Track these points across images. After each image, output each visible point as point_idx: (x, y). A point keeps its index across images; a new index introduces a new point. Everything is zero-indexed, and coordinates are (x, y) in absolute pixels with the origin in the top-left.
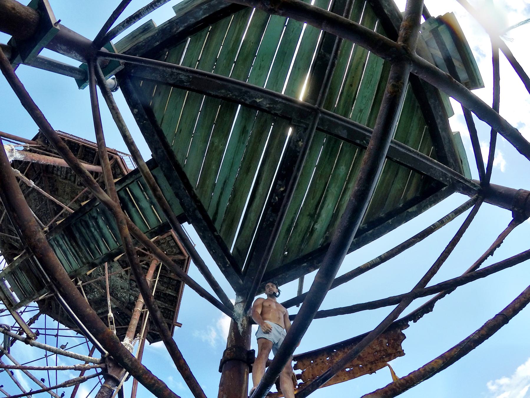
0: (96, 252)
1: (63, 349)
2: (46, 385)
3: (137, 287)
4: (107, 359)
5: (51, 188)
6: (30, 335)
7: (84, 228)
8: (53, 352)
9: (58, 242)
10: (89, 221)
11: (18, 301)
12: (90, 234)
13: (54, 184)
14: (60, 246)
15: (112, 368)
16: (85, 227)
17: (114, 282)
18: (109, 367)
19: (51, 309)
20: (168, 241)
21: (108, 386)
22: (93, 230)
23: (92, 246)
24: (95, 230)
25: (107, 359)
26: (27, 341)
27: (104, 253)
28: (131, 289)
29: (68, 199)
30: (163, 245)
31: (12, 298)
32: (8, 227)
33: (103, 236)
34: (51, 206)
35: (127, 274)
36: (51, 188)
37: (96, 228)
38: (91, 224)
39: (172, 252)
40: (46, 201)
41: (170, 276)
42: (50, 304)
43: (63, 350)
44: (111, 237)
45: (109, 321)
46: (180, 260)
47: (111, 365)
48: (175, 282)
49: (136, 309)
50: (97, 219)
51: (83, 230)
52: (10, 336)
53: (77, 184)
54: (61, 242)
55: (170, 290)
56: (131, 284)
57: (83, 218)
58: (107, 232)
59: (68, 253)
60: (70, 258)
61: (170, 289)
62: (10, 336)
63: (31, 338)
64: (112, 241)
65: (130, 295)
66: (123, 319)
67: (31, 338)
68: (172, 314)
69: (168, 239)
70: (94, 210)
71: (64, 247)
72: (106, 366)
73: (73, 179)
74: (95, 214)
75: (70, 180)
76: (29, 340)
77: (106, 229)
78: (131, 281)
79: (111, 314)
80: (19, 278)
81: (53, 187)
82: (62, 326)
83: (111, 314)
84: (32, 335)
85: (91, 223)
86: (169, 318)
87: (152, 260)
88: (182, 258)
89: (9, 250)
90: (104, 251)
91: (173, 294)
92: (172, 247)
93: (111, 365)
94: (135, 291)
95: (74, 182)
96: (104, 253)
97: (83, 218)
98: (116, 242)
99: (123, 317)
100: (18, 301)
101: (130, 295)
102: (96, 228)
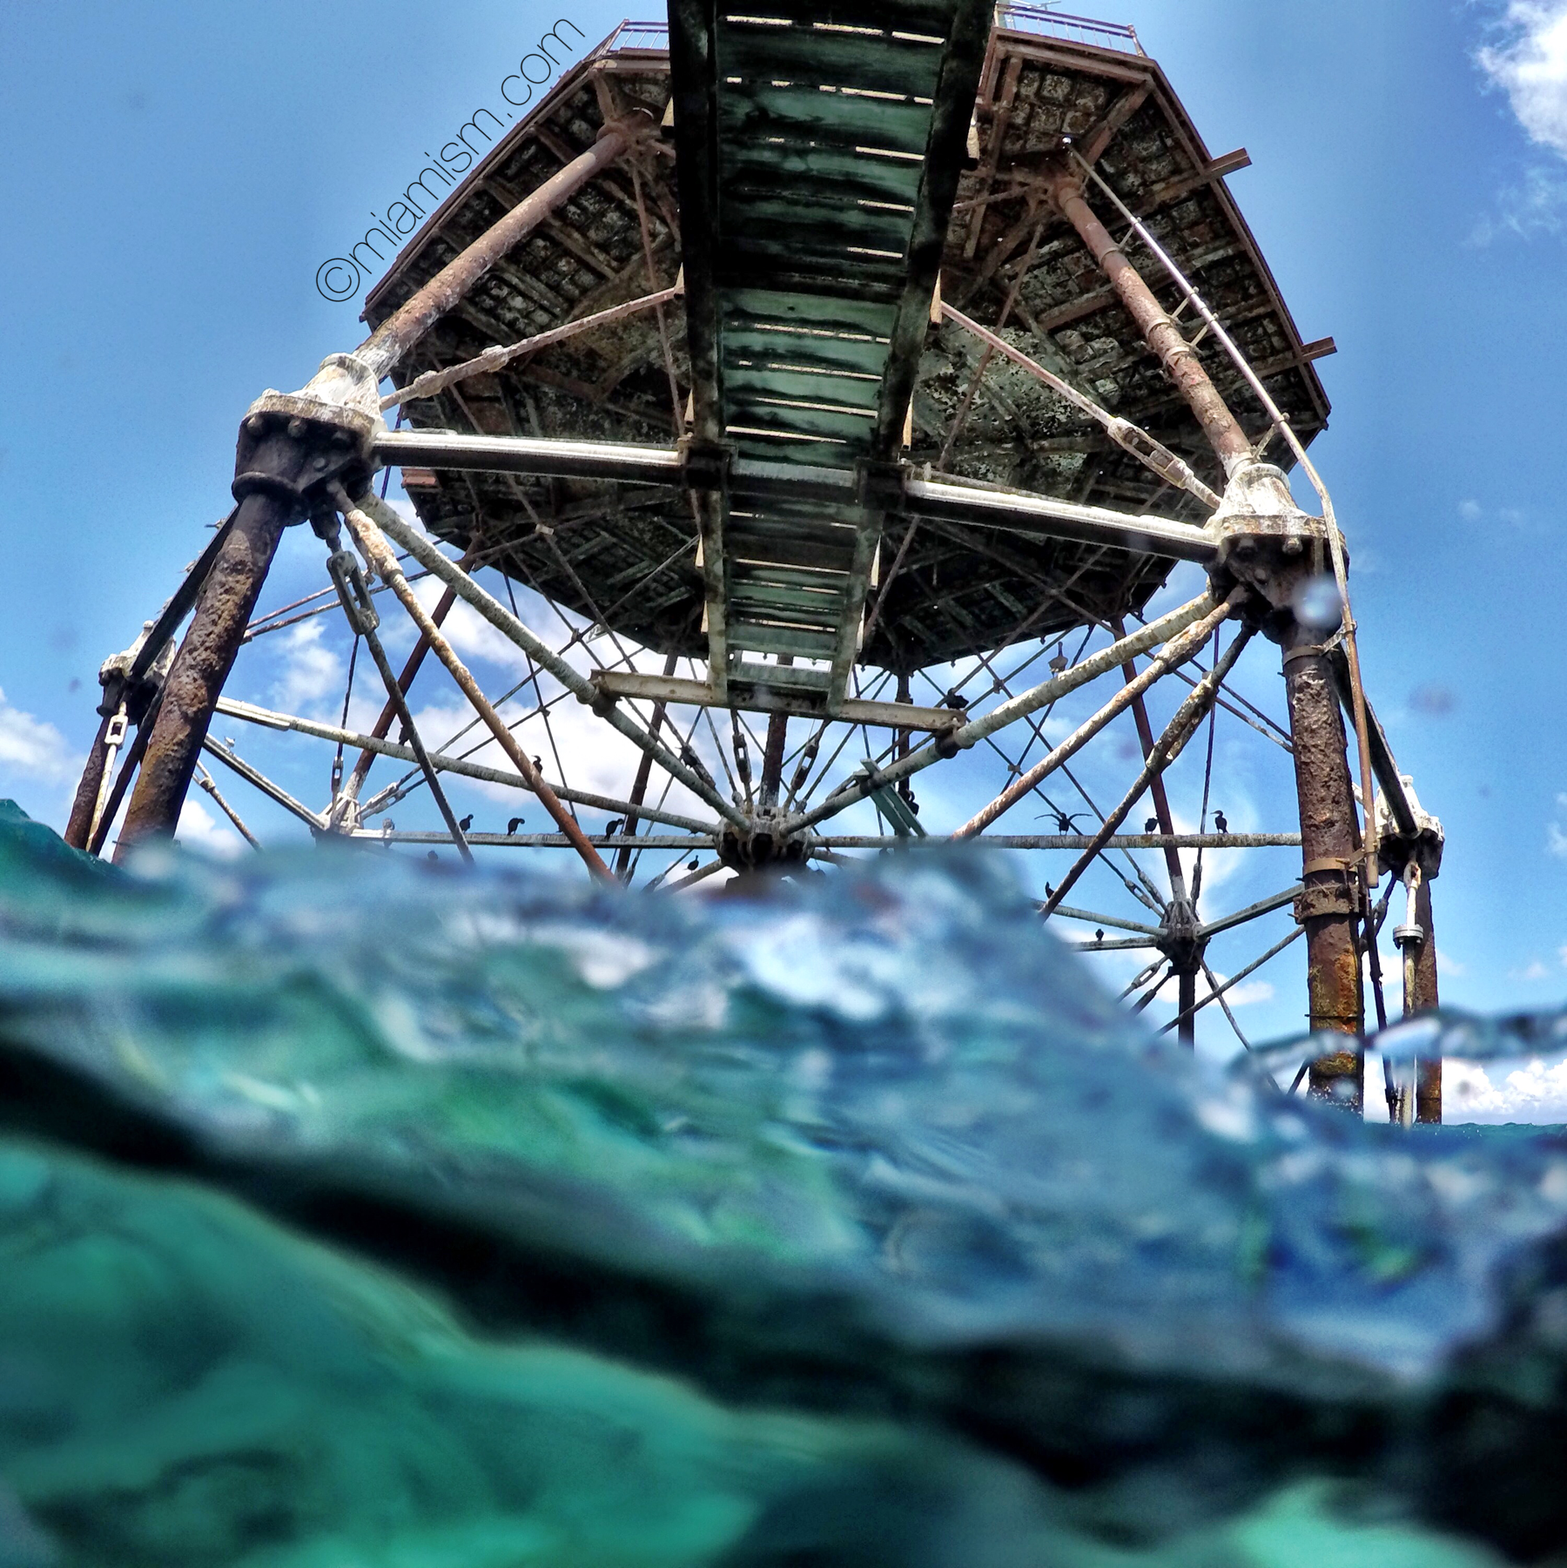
0: (883, 222)
1: (1062, 669)
2: (1092, 827)
3: (1088, 338)
4: (1235, 565)
5: (575, 373)
6: (938, 724)
7: (767, 199)
8: (1042, 705)
9: (745, 352)
10: (755, 155)
11: (824, 666)
12: (804, 193)
13: (569, 356)
14: (764, 357)
15: (1272, 583)
16: (763, 191)
17: (1011, 394)
18: (1262, 582)
19: (919, 641)
20: (1038, 93)
21: (1302, 651)
22: (794, 164)
23: (853, 219)
24: (802, 153)
25: (1235, 565)
26: (946, 746)
27: (911, 192)
28: (1078, 363)
29: (644, 336)
30: (1035, 125)
31: (803, 678)
32: (612, 587)
33: (842, 139)
34: (632, 406)
35: (1027, 329)
36: (575, 373)
37: (799, 144)
38: (767, 156)
39: (1087, 114)
40: (607, 412)
41: (1158, 199)
42: (904, 634)
43: (1068, 672)
44: (876, 108)
45: (1130, 449)
46: (1137, 115)
47: (1261, 573)
48: (1191, 206)
49: (1169, 358)
50: (763, 111)
51: (770, 209)
52: (890, 781)
53: (617, 271)
54: (756, 341)
55: (1200, 250)
56: (1064, 349)
57: (727, 172)
58: (847, 107)
59: (810, 345)
60: (833, 350)
61: (1195, 245)
62: (890, 781)
63: (949, 731)
64: (896, 121)
65: (1092, 382)
66: (1136, 479)
67: (949, 731)
68: (1271, 328)
69: (1028, 91)
70: (724, 100)
71: (781, 344)
72: (1249, 587)
73: (587, 278)
74: (743, 109)
75: (584, 291)
76: (948, 741)
77: (833, 104)
78: (1058, 337)
79: (1116, 425)
80: (765, 604)
81: (576, 363)
82: (985, 655)
83: (1116, 425)
84: (946, 718)
85: (768, 149)
86: (1275, 351)
87: (1056, 198)
88: (1137, 100)
89: (674, 628)
90: (902, 182)
91: (1220, 254)
92: (1068, 104)
93: (1261, 573)
94: (1094, 357)
95: (601, 277)
96: (911, 192)
97: (727, 172)
98: (909, 103)
99: (1130, 473)
100: (824, 666)
101: (1092, 382)
102: (799, 144)
